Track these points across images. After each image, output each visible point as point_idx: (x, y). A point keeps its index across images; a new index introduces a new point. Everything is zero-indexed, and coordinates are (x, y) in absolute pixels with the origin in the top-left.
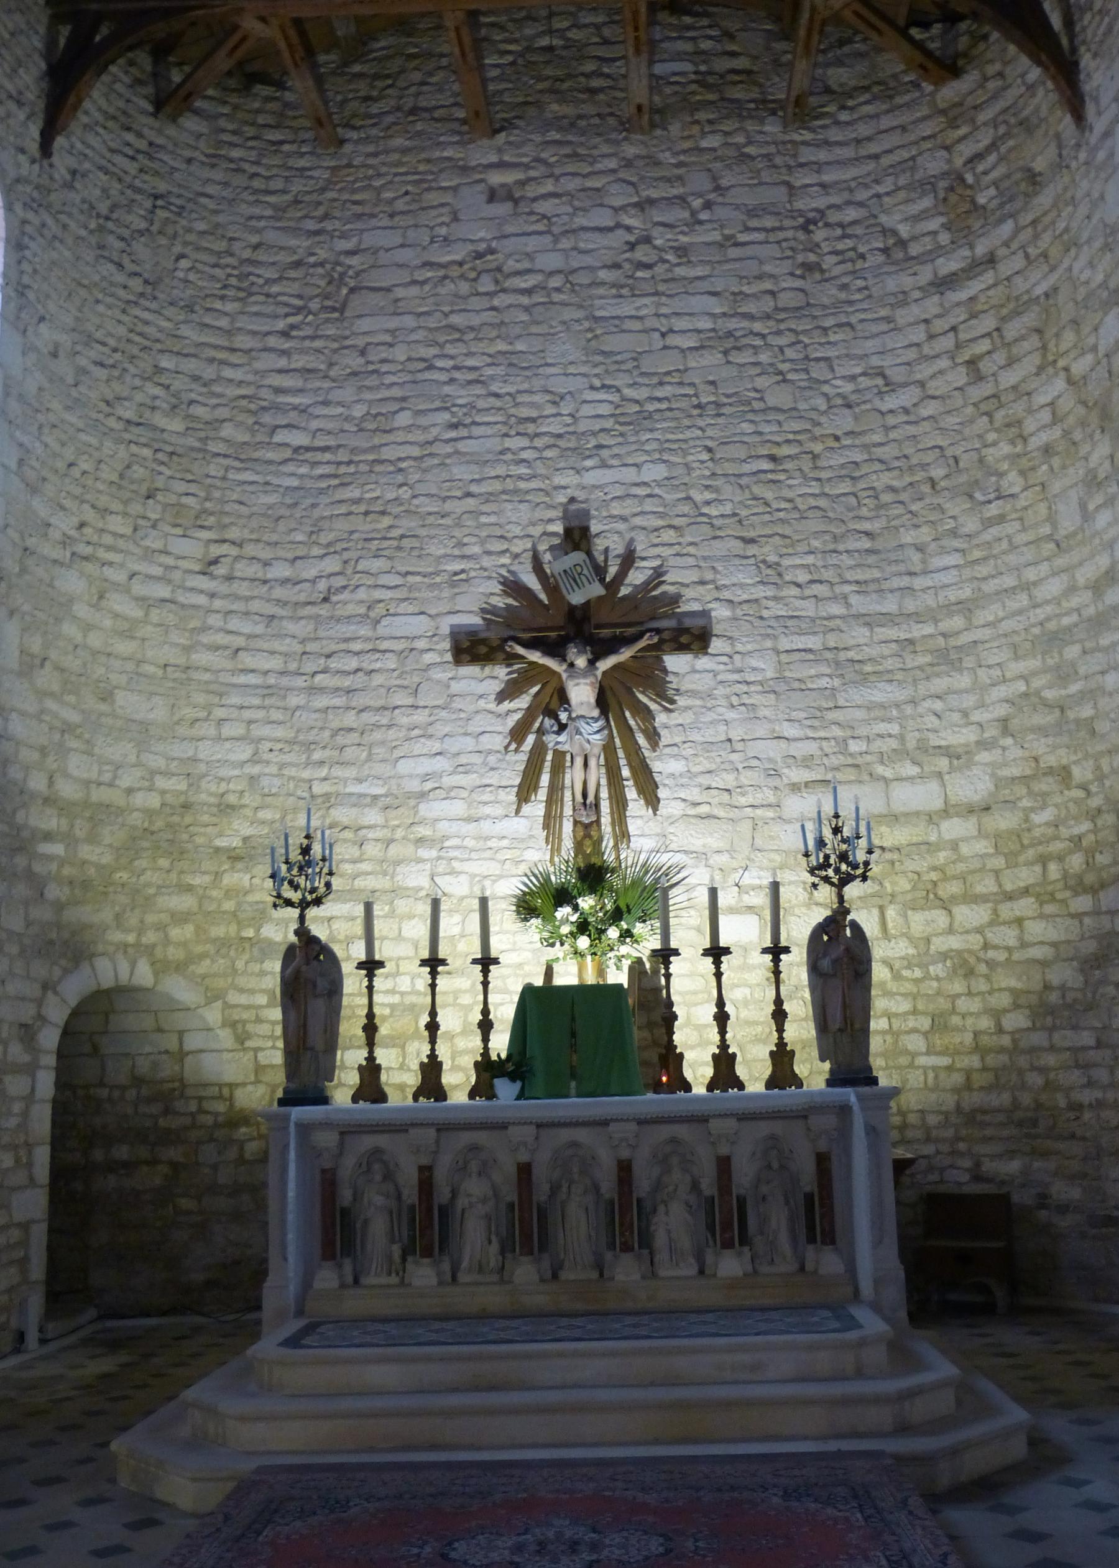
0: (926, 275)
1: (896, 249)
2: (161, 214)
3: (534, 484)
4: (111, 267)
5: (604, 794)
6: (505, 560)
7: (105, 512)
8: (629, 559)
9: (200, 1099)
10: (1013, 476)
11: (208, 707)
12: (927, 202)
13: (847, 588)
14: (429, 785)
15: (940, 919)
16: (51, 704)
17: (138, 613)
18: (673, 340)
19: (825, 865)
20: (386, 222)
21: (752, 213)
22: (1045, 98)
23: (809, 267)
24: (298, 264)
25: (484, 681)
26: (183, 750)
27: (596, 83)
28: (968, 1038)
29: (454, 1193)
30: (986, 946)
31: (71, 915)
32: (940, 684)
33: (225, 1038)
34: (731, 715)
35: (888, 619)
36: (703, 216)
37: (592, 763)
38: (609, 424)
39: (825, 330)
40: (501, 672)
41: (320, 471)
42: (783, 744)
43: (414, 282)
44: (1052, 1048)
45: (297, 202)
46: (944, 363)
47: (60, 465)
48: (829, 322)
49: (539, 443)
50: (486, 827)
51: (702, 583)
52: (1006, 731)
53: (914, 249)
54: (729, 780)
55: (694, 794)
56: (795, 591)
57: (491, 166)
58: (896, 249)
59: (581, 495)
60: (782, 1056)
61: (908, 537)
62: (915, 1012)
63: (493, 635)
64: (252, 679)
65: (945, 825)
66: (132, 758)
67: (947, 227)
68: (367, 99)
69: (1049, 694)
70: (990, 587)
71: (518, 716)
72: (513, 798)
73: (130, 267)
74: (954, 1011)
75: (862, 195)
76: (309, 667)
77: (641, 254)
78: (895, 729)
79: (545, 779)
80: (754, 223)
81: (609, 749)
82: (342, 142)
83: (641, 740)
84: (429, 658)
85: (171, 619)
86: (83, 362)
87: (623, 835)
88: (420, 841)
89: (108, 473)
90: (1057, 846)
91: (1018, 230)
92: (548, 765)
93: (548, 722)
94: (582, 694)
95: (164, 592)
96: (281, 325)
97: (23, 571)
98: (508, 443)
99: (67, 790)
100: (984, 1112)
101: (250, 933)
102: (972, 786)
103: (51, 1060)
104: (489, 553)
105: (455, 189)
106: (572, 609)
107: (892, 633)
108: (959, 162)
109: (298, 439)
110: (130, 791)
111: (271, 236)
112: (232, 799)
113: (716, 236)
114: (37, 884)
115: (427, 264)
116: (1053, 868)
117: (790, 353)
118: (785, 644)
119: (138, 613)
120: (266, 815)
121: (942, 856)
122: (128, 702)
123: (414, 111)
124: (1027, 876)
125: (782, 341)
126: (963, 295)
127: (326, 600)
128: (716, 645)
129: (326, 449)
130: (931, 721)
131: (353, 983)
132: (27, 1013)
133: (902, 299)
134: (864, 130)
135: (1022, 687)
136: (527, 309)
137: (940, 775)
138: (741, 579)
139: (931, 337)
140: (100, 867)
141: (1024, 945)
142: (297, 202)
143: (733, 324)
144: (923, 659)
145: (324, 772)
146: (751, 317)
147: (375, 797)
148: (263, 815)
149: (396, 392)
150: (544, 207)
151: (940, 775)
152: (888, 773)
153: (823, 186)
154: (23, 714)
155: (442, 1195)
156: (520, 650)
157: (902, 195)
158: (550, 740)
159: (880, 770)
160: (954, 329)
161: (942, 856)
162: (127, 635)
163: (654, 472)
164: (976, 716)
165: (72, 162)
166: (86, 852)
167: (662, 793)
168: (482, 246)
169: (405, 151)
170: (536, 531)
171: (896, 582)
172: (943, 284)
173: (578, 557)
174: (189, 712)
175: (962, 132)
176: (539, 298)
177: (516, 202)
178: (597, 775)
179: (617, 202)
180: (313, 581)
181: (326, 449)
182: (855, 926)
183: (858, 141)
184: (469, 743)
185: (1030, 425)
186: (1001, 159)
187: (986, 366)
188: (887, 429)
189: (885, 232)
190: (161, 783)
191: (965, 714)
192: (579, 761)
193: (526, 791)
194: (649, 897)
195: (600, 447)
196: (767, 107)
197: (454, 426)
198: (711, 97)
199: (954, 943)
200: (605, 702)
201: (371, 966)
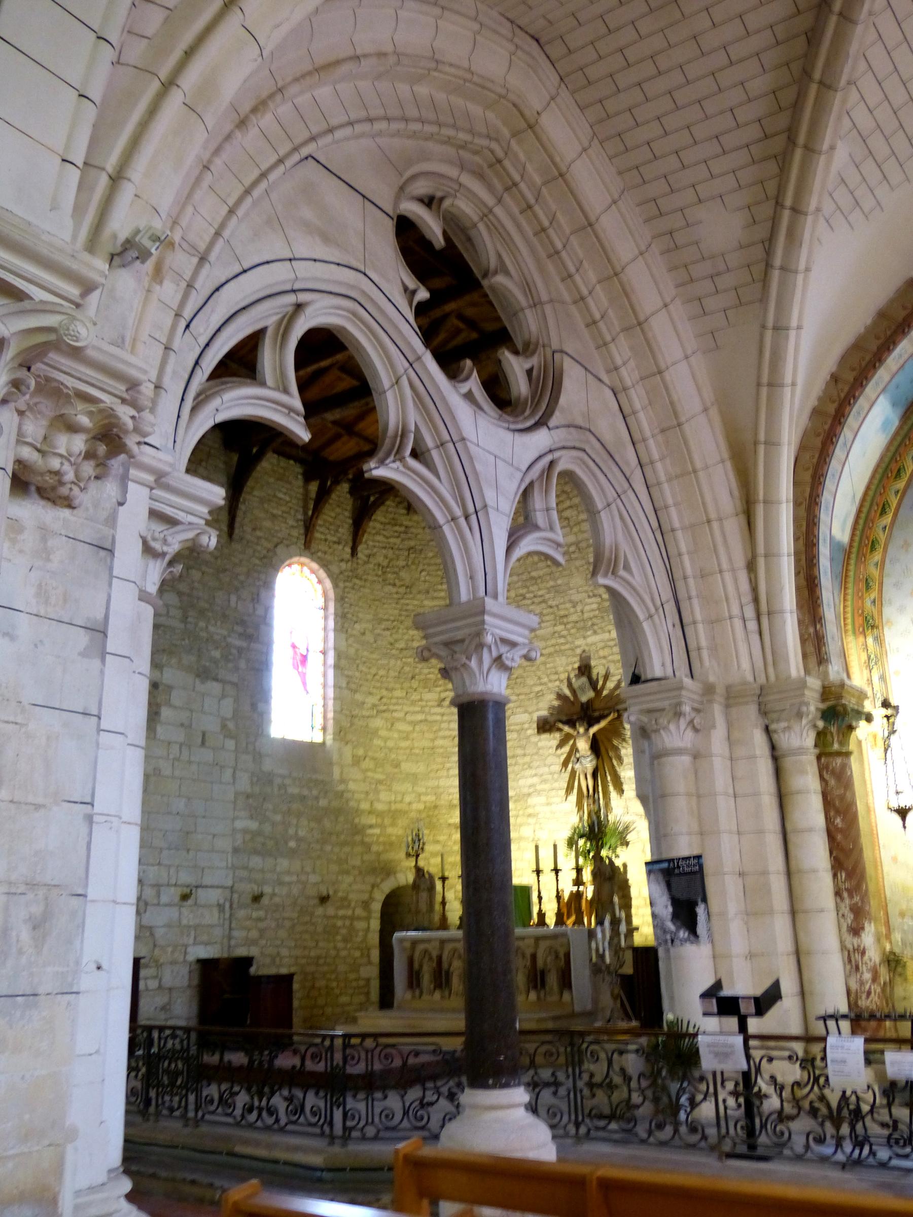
2: (412, 556)
3: (567, 646)
4: (390, 587)
6: (557, 683)
7: (392, 690)
8: (606, 677)
11: (443, 764)
14: (531, 790)
16: (369, 774)
17: (410, 728)
25: (550, 740)
26: (431, 783)
29: (450, 965)
31: (384, 857)
40: (557, 736)
47: (369, 677)
49: (569, 626)
59: (587, 648)
63: (552, 720)
66: (410, 789)
84: (529, 732)
85: (425, 728)
86: (378, 631)
88: (530, 815)
89: (392, 674)
94: (583, 745)
95: (420, 717)
97: (352, 724)
98: (556, 628)
99: (380, 807)
104: (550, 681)
106: (582, 704)
110: (410, 803)
114: (367, 847)
119: (410, 728)
122: (406, 767)
132: (365, 897)
140: (397, 836)
154: (354, 781)
155: (445, 965)
162: (406, 738)
165: (367, 552)
166: (390, 830)
170: (570, 668)
174: (435, 767)
184: (546, 769)
190: (423, 798)
193: (569, 789)
195: (593, 625)
200: (595, 747)
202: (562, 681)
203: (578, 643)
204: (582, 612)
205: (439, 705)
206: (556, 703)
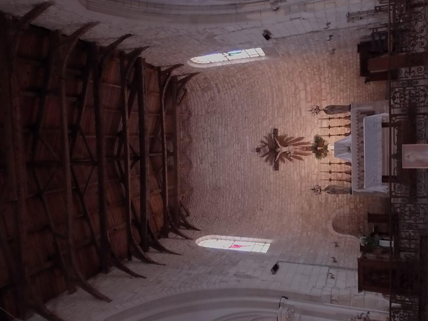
0: (217, 94)
1: (212, 99)
3: (249, 157)
5: (301, 146)
6: (261, 162)
8: (262, 142)
9: (352, 214)
10: (251, 80)
12: (206, 94)
13: (267, 106)
15: (323, 91)
18: (226, 134)
19: (316, 112)
20: (205, 181)
21: (205, 122)
22: (194, 78)
23: (214, 113)
24: (212, 195)
25: (282, 166)
27: (184, 147)
28: (344, 86)
30: (329, 83)
32: (284, 91)
33: (341, 210)
34: (288, 125)
35: (273, 100)
36: (206, 129)
37: (296, 148)
38: (239, 145)
39: (225, 110)
40: (280, 162)
41: (245, 192)
42: (293, 117)
43: (215, 176)
44: (347, 72)
45: (202, 195)
46: (232, 91)
48: (223, 109)
49: (242, 156)
50: (306, 165)
51: (266, 130)
52: (292, 81)
53: (213, 96)
54: (299, 126)
55: (301, 131)
56: (268, 115)
57: (197, 163)
58: (212, 99)
59: (251, 149)
60: (346, 118)
61: (259, 96)
62: (340, 95)
63: (274, 164)
64: (280, 204)
65: (308, 90)
67: (210, 91)
68: (185, 183)
69: (287, 74)
70: (269, 84)
71: (288, 160)
72: (301, 161)
73: (214, 220)
74: (340, 88)
75: (203, 104)
76: (278, 194)
77: (212, 139)
78: (291, 98)
79: (298, 156)
80: (207, 121)
81: (294, 145)
82: (192, 187)
83: (292, 140)
84: (277, 174)
86: (230, 227)
87: (308, 143)
88: (308, 176)
90: (312, 72)
91: (212, 80)
92: (296, 155)
93: (289, 155)
94: (285, 149)
96: (222, 198)
100: (358, 83)
101: (323, 205)
102: (301, 86)
103: (345, 235)
105: (200, 169)
106: (270, 151)
107: (275, 99)
108: (200, 89)
109: (240, 195)
110: (299, 223)
111: (207, 199)
112: (300, 207)
113: (209, 127)
115: (212, 174)
116: (316, 73)
117: (228, 115)
118: (276, 116)
120: (303, 202)
121: (313, 90)
123: (187, 176)
124: (317, 77)
125: (226, 117)
126: (221, 88)
127: (267, 191)
128: (276, 128)
129: (242, 191)
130: (290, 92)
131: (333, 183)
133: (221, 98)
134: (193, 104)
135: (285, 79)
136: (220, 158)
137: (299, 91)
138: (265, 123)
139: (227, 93)
141: (329, 77)
142: (202, 195)
143: (223, 125)
144: (280, 94)
145: (296, 192)
146: (222, 121)
147: (301, 184)
148: (303, 202)
149: (233, 179)
150: (204, 155)
151: (299, 91)
152: (299, 99)
153: (201, 110)
156: (277, 159)
157: (204, 98)
158: (292, 154)
159: (298, 101)
160: (226, 90)
161: (313, 90)
163: (247, 137)
164: (290, 85)
167: (301, 136)
168: (210, 165)
169: (194, 177)
170: (256, 157)
171: (267, 98)
172: (219, 91)
173: (261, 150)
175: (195, 89)
176: (218, 156)
177: (203, 159)
178: (298, 147)
179: (203, 143)
180: (264, 193)
181: (242, 191)
182: (326, 108)
183: (194, 105)
184: (292, 168)
185: (243, 78)
186: (201, 83)
187: (233, 85)
188: (241, 100)
189: (209, 100)
190: (298, 218)
191: (289, 87)
192: (296, 150)
193: (300, 159)
194: (319, 141)
196: (188, 119)
197: (239, 170)
198: (186, 128)
199: (328, 88)
201: (330, 180)
202: (261, 160)
203: (248, 152)
204: (238, 151)
205: (263, 211)
206: (269, 163)
